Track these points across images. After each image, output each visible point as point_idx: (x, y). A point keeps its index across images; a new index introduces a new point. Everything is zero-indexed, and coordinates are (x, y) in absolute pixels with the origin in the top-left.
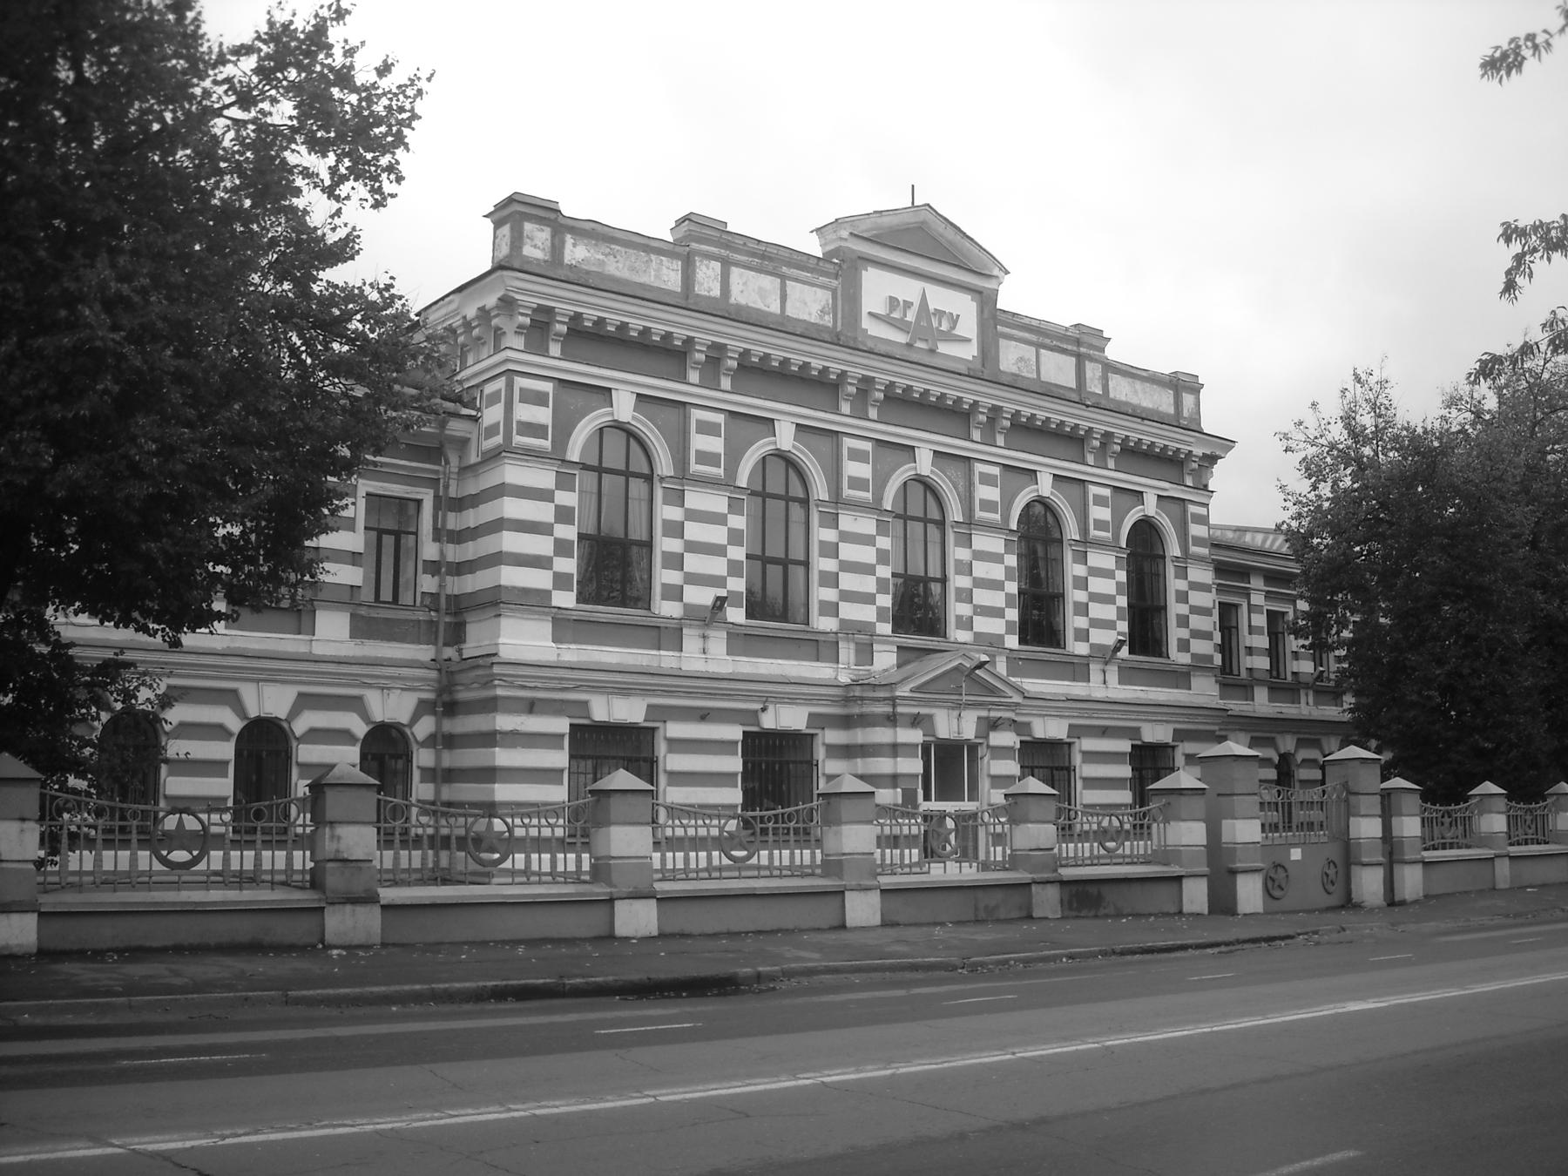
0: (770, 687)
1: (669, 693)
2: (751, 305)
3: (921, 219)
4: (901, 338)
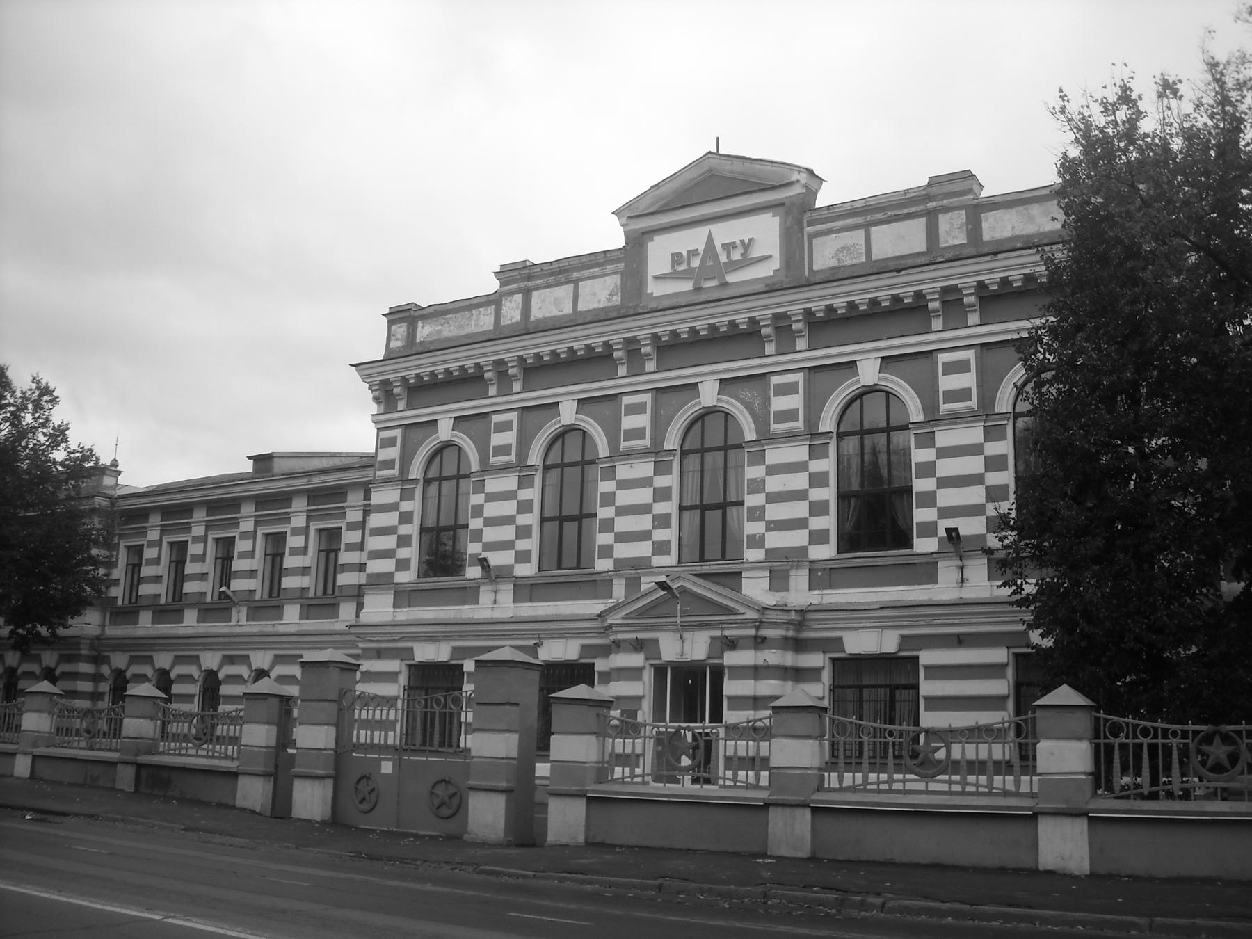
0: (544, 626)
1: (462, 637)
2: (547, 315)
3: (706, 169)
4: (687, 286)
